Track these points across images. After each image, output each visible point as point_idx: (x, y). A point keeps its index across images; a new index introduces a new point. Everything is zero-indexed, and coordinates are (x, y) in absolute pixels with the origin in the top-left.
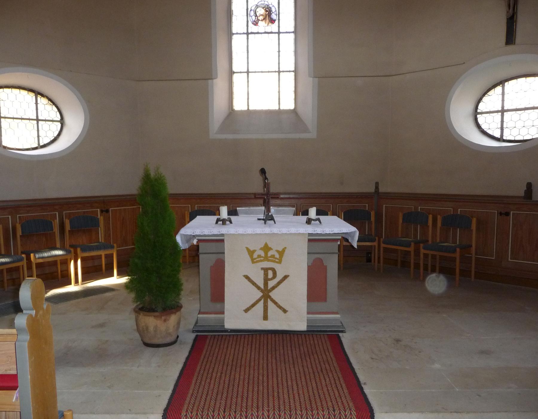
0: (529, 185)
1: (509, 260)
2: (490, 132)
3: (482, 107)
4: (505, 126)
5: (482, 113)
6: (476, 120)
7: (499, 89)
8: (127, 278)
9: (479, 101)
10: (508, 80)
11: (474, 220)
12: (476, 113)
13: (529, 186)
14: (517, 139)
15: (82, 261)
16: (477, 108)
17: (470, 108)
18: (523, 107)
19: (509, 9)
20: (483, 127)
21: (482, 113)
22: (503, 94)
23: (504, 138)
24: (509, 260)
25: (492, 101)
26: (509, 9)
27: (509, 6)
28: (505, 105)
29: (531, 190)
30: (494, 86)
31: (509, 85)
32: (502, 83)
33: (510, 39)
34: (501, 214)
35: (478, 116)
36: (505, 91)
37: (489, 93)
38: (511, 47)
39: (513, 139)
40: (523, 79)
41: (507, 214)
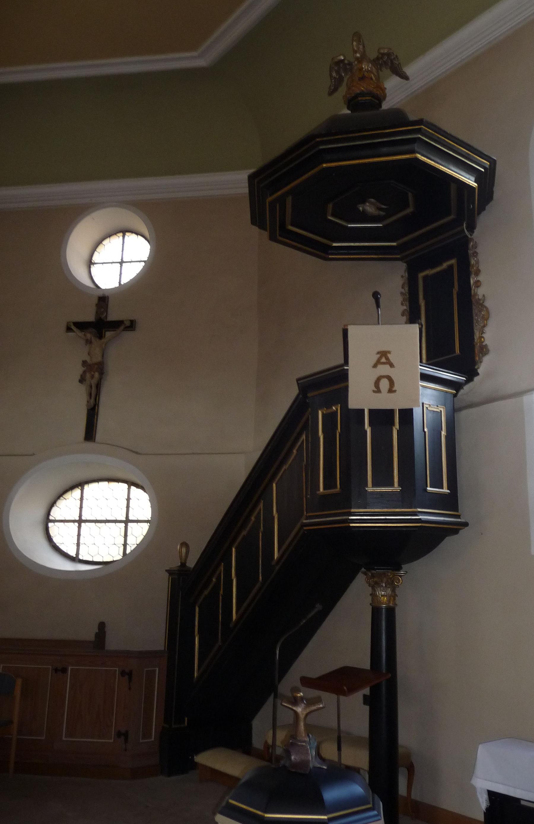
0: (102, 626)
1: (64, 739)
2: (63, 548)
3: (55, 513)
4: (81, 541)
5: (54, 521)
6: (47, 529)
7: (77, 492)
8: (362, 790)
9: (53, 504)
10: (88, 482)
11: (19, 682)
12: (47, 520)
13: (102, 626)
14: (96, 559)
15: (194, 676)
16: (48, 514)
17: (40, 513)
18: (104, 518)
19: (91, 398)
20: (56, 540)
21: (54, 521)
22: (82, 499)
23: (81, 557)
24: (64, 739)
25: (67, 507)
26: (91, 398)
27: (90, 395)
28: (83, 514)
29: (105, 632)
30: (72, 488)
31: (89, 489)
32: (81, 485)
33: (90, 434)
34: (56, 670)
35: (50, 525)
36: (84, 495)
37: (65, 496)
38: (90, 445)
39: (90, 559)
40: (105, 484)
41: (64, 670)
